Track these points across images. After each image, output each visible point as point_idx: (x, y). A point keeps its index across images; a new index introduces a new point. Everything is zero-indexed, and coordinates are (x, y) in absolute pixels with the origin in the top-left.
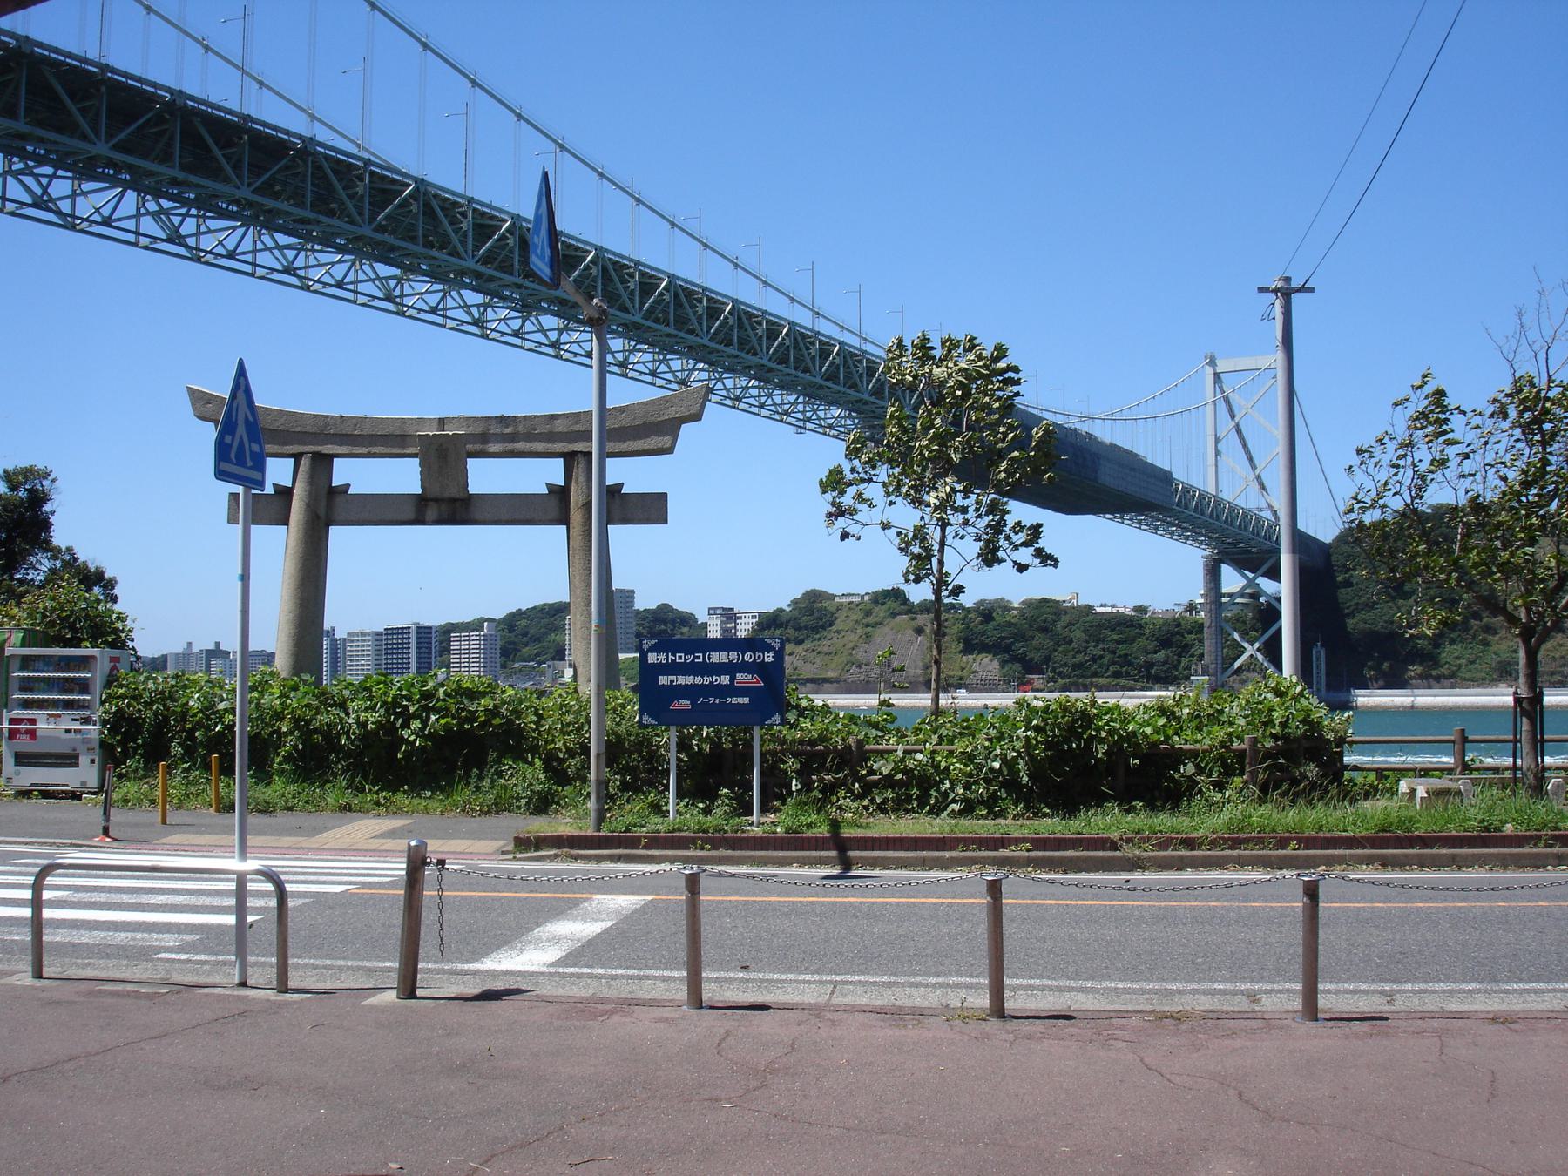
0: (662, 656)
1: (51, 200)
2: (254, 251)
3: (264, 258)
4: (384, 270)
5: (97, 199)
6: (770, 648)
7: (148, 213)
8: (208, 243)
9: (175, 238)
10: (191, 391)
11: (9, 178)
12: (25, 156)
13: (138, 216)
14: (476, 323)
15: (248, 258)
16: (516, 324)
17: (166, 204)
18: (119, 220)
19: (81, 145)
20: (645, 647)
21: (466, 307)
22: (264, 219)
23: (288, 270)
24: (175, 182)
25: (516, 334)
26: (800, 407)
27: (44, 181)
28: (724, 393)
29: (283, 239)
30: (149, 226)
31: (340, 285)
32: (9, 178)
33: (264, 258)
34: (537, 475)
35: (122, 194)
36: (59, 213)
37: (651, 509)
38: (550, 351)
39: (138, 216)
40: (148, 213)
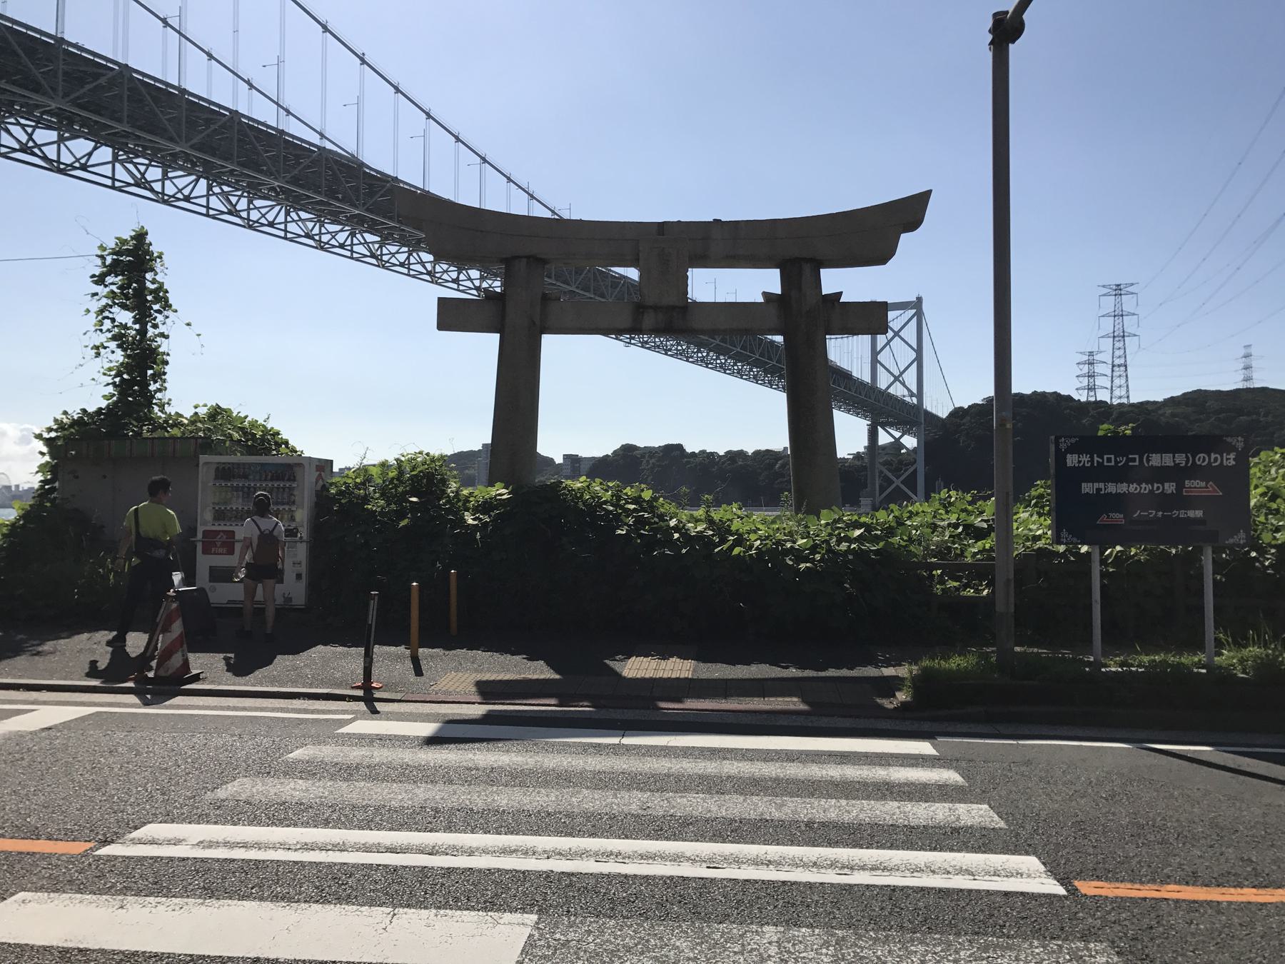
0: (1085, 459)
1: (37, 146)
2: (286, 222)
4: (369, 237)
5: (181, 181)
6: (1231, 448)
7: (214, 194)
9: (233, 212)
11: (118, 165)
13: (208, 196)
14: (429, 273)
15: (282, 226)
16: (454, 275)
17: (226, 188)
20: (1063, 447)
21: (422, 263)
22: (212, 175)
23: (307, 236)
24: (231, 172)
25: (454, 281)
29: (304, 215)
30: (215, 203)
31: (342, 246)
32: (118, 165)
33: (292, 227)
34: (753, 284)
35: (197, 181)
36: (45, 158)
37: (871, 318)
38: (427, 278)
40: (214, 194)
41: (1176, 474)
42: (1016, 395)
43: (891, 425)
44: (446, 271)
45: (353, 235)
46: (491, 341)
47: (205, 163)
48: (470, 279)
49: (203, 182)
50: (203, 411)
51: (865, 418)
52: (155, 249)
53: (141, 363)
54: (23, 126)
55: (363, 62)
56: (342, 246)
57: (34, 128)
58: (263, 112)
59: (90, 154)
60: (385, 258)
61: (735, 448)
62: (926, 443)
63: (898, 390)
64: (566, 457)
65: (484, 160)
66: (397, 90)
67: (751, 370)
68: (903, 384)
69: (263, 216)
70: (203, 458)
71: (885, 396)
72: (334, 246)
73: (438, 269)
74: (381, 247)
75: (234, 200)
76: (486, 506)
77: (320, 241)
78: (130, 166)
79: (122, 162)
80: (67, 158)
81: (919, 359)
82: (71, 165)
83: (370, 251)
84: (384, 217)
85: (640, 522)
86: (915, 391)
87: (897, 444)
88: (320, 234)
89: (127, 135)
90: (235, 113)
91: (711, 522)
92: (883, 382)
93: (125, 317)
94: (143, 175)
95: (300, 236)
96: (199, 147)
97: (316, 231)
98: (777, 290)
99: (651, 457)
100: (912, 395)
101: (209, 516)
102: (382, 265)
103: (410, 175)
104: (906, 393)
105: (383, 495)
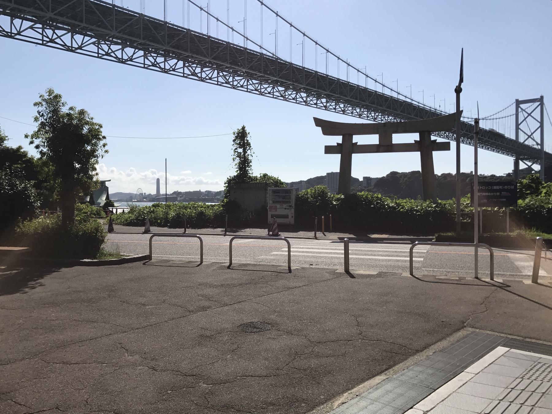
1: (158, 63)
2: (247, 85)
3: (220, 79)
4: (281, 89)
5: (207, 72)
6: (512, 185)
8: (204, 75)
10: (243, 128)
12: (188, 62)
13: (218, 77)
14: (304, 102)
16: (315, 102)
17: (225, 73)
18: (134, 59)
19: (109, 32)
21: (302, 98)
22: (220, 69)
23: (256, 90)
26: (380, 117)
27: (194, 68)
28: (340, 109)
29: (255, 81)
30: (220, 79)
31: (269, 93)
32: (185, 68)
33: (250, 87)
36: (160, 68)
38: (304, 103)
39: (218, 77)
41: (500, 191)
42: (462, 173)
43: (526, 159)
44: (312, 100)
45: (273, 88)
46: (339, 156)
47: (217, 64)
48: (322, 103)
49: (216, 71)
50: (262, 175)
51: (513, 156)
52: (247, 132)
53: (244, 164)
54: (153, 57)
55: (277, 15)
56: (269, 93)
57: (157, 57)
58: (238, 41)
59: (176, 64)
60: (287, 97)
61: (446, 172)
62: (545, 168)
63: (530, 142)
64: (364, 178)
65: (328, 51)
66: (291, 25)
67: (453, 135)
68: (534, 140)
69: (239, 83)
70: (269, 188)
71: (523, 145)
72: (266, 93)
73: (308, 99)
74: (285, 92)
75: (227, 78)
76: (338, 200)
77: (261, 92)
78: (190, 68)
79: (187, 67)
80: (168, 67)
81: (542, 126)
82: (169, 69)
83: (281, 94)
84: (286, 80)
85: (377, 203)
86: (539, 142)
87: (530, 169)
88: (261, 89)
89: (188, 56)
90: (228, 43)
91: (396, 203)
92: (522, 139)
93: (240, 150)
94: (194, 71)
95: (253, 90)
96: (214, 58)
97: (259, 88)
98: (418, 139)
99: (405, 177)
100: (538, 144)
101: (271, 202)
102: (286, 99)
103: (297, 61)
104: (535, 143)
105: (312, 197)
